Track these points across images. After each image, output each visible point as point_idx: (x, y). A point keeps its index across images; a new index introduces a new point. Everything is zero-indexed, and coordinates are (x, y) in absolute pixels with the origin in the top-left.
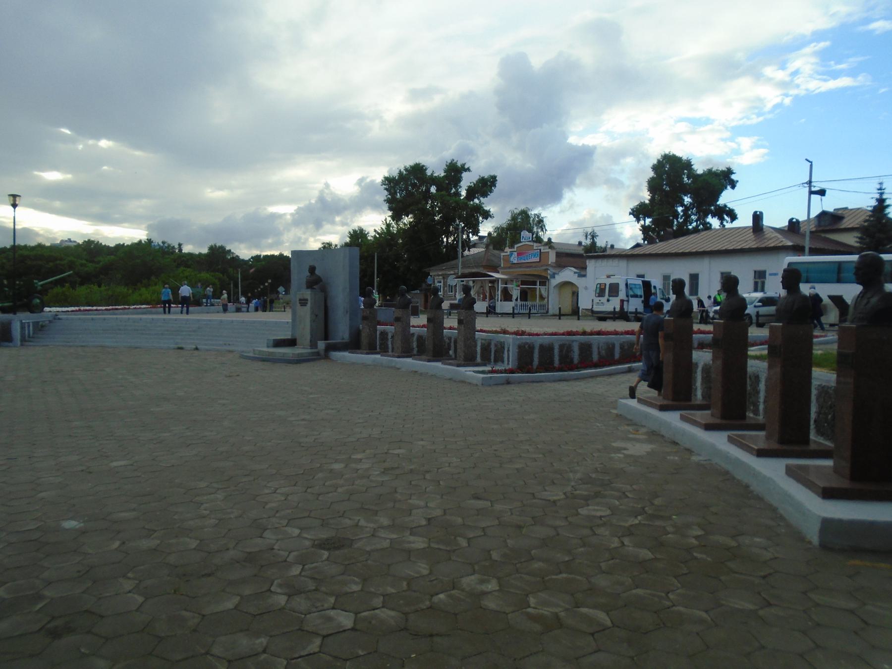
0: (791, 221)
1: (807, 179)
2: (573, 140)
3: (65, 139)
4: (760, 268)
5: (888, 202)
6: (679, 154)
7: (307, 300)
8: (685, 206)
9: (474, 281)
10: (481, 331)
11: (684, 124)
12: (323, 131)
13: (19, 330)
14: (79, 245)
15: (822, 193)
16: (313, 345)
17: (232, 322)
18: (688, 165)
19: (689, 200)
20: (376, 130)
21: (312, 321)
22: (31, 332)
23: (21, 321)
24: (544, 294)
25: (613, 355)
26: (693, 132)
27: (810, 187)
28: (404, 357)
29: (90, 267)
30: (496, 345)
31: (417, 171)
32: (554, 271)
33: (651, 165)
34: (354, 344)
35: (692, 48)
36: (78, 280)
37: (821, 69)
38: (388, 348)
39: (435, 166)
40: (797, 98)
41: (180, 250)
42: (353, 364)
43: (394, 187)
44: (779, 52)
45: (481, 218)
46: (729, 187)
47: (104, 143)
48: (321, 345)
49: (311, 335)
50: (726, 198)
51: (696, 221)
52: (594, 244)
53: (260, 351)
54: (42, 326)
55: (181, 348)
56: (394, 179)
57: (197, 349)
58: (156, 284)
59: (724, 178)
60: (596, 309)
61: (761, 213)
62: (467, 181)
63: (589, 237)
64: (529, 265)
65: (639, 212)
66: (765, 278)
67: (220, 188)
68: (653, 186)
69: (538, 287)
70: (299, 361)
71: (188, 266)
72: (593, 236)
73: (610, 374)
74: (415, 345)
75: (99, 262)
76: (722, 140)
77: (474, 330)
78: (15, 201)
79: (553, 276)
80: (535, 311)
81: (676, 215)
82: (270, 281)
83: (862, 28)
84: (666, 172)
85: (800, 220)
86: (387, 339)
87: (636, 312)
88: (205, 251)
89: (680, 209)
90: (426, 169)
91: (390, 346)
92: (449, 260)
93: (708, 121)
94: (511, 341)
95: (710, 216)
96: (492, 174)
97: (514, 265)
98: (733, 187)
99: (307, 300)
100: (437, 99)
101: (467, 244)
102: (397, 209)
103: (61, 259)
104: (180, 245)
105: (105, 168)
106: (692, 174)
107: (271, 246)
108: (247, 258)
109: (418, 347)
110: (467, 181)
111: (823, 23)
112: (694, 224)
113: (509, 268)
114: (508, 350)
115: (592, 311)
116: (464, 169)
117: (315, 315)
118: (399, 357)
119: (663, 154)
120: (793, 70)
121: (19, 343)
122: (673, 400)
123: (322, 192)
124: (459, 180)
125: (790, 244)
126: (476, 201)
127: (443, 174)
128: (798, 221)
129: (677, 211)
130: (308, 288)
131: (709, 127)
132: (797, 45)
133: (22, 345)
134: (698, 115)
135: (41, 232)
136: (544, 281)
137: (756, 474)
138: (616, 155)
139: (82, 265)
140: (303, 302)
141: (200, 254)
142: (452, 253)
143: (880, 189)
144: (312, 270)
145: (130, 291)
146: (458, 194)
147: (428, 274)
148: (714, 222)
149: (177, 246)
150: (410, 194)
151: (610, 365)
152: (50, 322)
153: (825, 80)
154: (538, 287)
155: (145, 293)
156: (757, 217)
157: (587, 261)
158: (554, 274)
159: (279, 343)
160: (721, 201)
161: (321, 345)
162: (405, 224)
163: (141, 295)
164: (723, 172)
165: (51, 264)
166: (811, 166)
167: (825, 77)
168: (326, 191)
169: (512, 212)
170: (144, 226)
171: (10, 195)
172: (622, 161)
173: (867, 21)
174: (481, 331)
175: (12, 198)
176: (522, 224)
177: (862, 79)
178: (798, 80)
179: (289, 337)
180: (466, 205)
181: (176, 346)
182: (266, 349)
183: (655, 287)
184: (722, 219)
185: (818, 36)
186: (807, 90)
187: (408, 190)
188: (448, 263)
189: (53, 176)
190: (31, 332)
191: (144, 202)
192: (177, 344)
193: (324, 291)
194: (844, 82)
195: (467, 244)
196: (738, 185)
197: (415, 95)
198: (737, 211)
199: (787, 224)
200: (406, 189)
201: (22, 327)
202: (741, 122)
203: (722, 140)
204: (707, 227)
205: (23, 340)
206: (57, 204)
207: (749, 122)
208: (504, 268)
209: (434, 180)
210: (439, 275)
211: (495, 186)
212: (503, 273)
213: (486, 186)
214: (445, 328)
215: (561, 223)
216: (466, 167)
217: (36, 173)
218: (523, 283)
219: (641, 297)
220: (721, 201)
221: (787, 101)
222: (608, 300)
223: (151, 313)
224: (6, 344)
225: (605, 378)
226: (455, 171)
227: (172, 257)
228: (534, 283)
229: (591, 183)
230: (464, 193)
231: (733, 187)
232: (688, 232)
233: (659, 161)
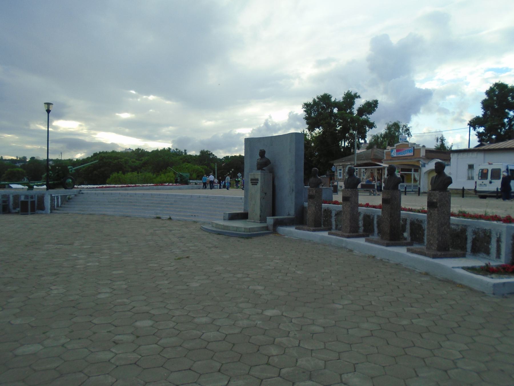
2: (418, 85)
3: (132, 96)
7: (257, 180)
9: (366, 169)
11: (491, 72)
12: (266, 87)
13: (49, 201)
14: (133, 151)
16: (263, 219)
17: (200, 197)
20: (296, 85)
21: (262, 198)
22: (60, 204)
23: (51, 195)
24: (417, 178)
29: (138, 163)
30: (475, 233)
31: (326, 98)
32: (424, 162)
33: (485, 91)
34: (299, 220)
35: (496, 26)
36: (130, 169)
38: (331, 225)
39: (338, 96)
41: (186, 153)
42: (301, 240)
43: (310, 110)
45: (367, 128)
47: (151, 98)
48: (270, 220)
49: (261, 210)
52: (443, 145)
53: (217, 224)
54: (69, 199)
55: (159, 218)
56: (310, 104)
57: (170, 219)
58: (169, 172)
60: (478, 189)
62: (359, 103)
63: (439, 140)
64: (405, 158)
65: (474, 123)
67: (210, 120)
68: (486, 105)
69: (413, 173)
70: (249, 235)
71: (189, 162)
72: (442, 140)
74: (361, 223)
75: (141, 160)
77: (399, 208)
78: (48, 107)
79: (424, 165)
80: (410, 190)
81: (504, 125)
82: (233, 170)
84: (496, 95)
86: (331, 217)
88: (198, 154)
90: (331, 97)
91: (334, 223)
92: (346, 156)
94: (504, 230)
96: (375, 99)
97: (393, 158)
99: (257, 180)
100: (333, 65)
101: (359, 146)
102: (312, 123)
103: (121, 158)
104: (185, 151)
105: (151, 110)
107: (237, 151)
108: (221, 158)
109: (364, 225)
110: (359, 103)
113: (391, 160)
114: (499, 241)
115: (475, 191)
116: (356, 96)
117: (264, 193)
118: (348, 237)
121: (49, 211)
123: (267, 120)
124: (353, 103)
126: (364, 117)
127: (342, 100)
130: (258, 169)
131: (508, 73)
133: (51, 212)
134: (500, 66)
135: (120, 145)
136: (417, 169)
138: (444, 94)
139: (133, 162)
140: (254, 182)
141: (196, 155)
142: (348, 152)
144: (262, 154)
145: (155, 176)
146: (351, 113)
147: (333, 165)
149: (183, 151)
150: (320, 114)
152: (76, 195)
154: (413, 173)
155: (163, 177)
157: (451, 155)
158: (425, 164)
159: (233, 217)
161: (270, 220)
162: (316, 134)
163: (161, 178)
165: (116, 161)
168: (269, 120)
169: (388, 125)
170: (170, 142)
171: (45, 103)
172: (447, 98)
175: (46, 106)
176: (394, 134)
179: (242, 211)
180: (358, 119)
181: (155, 216)
182: (222, 223)
187: (320, 111)
188: (346, 157)
189: (125, 116)
190: (60, 204)
191: (171, 128)
192: (157, 214)
193: (272, 171)
195: (359, 146)
197: (320, 63)
200: (318, 110)
201: (52, 199)
205: (53, 208)
206: (127, 130)
208: (386, 160)
209: (336, 104)
210: (340, 165)
211: (377, 107)
212: (385, 163)
213: (371, 107)
214: (453, 215)
215: (422, 130)
216: (357, 95)
217: (117, 114)
218: (402, 170)
222: (491, 182)
223: (153, 189)
224: (41, 211)
226: (350, 98)
227: (180, 157)
228: (410, 170)
229: (429, 110)
230: (355, 112)
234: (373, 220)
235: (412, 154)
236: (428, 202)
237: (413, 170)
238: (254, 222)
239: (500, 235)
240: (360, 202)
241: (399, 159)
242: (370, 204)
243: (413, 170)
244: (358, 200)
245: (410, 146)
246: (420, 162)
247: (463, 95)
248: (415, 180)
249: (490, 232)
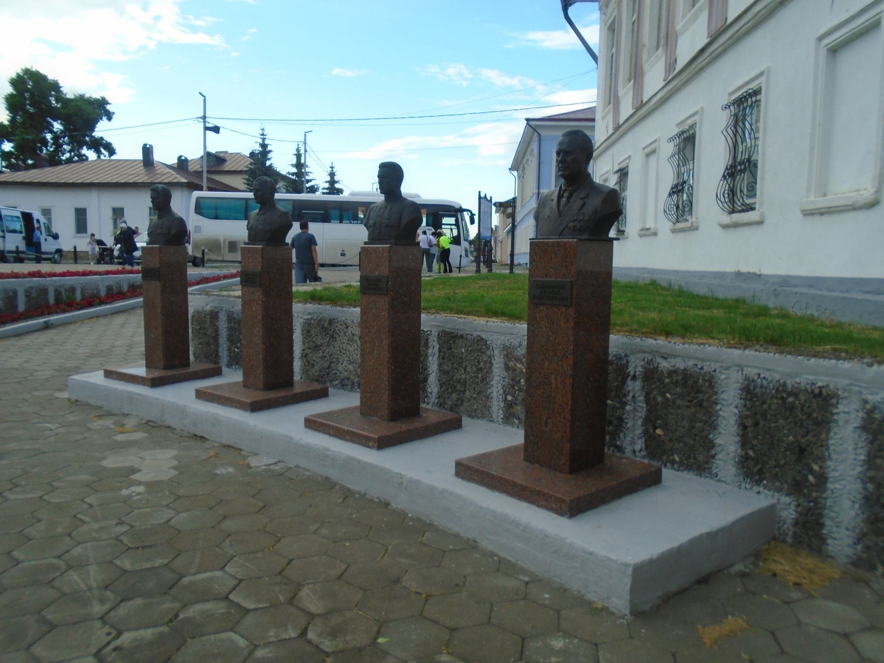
0: (180, 158)
1: (202, 114)
4: (81, 205)
5: (269, 148)
6: (43, 71)
8: (55, 133)
15: (216, 129)
18: (55, 87)
19: (61, 127)
25: (15, 306)
27: (205, 122)
46: (104, 118)
50: (102, 130)
51: (70, 152)
59: (98, 109)
61: (151, 146)
73: (18, 335)
81: (45, 142)
85: (189, 158)
87: (17, 251)
89: (49, 136)
95: (85, 148)
98: (110, 119)
106: (60, 97)
112: (68, 155)
119: (23, 67)
122: (166, 367)
125: (185, 181)
128: (186, 159)
129: (45, 137)
137: (401, 483)
143: (263, 135)
148: (91, 155)
151: (14, 320)
156: (147, 151)
160: (97, 134)
164: (97, 100)
166: (205, 100)
167: (185, 29)
177: (216, 40)
183: (38, 221)
184: (99, 152)
194: (201, 38)
196: (114, 117)
198: (115, 146)
199: (176, 161)
204: (83, 159)
219: (21, 232)
220: (97, 134)
225: (13, 341)
231: (110, 119)
232: (59, 163)
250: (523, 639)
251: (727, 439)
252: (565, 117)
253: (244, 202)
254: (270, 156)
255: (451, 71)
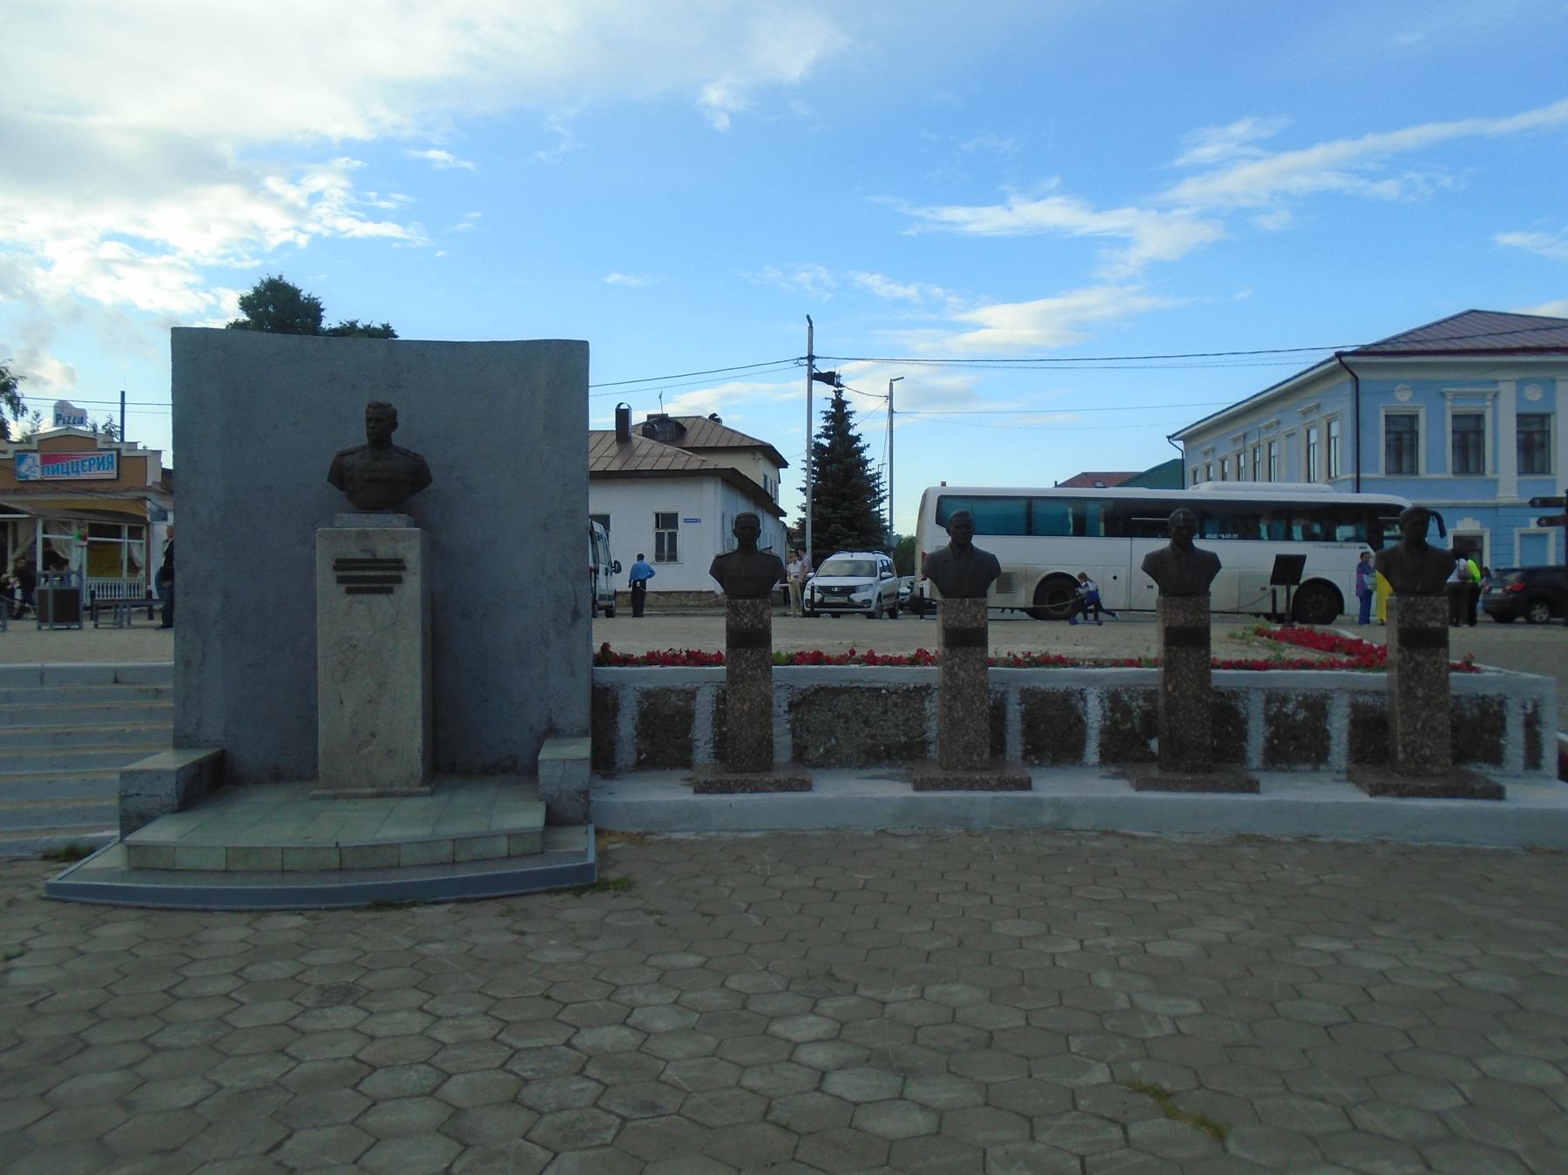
4: (666, 507)
7: (398, 564)
10: (1228, 665)
24: (140, 557)
26: (133, 263)
27: (811, 366)
28: (726, 788)
37: (354, 201)
40: (316, 239)
44: (296, 156)
64: (88, 486)
66: (676, 526)
69: (125, 540)
76: (190, 286)
83: (415, 153)
93: (162, 249)
99: (398, 564)
111: (358, 130)
119: (265, 278)
120: (313, 190)
131: (167, 259)
132: (319, 153)
134: (147, 234)
144: (382, 422)
153: (362, 220)
154: (125, 540)
173: (425, 145)
174: (1228, 665)
178: (321, 210)
185: (350, 147)
186: (334, 229)
194: (389, 230)
202: (223, 262)
203: (190, 286)
207: (237, 265)
218: (96, 530)
221: (302, 240)
228: (117, 532)
233: (257, 290)
234: (688, 717)
235: (111, 474)
236: (729, 631)
237: (125, 532)
238: (380, 795)
239: (1536, 706)
240: (991, 654)
241: (55, 491)
242: (878, 655)
243: (125, 532)
244: (176, 645)
245: (100, 446)
246: (148, 504)
247: (31, 297)
248: (133, 567)
249: (1502, 703)
250: (922, 997)
251: (1092, 752)
252: (1376, 349)
253: (1024, 503)
254: (852, 421)
255: (804, 277)
